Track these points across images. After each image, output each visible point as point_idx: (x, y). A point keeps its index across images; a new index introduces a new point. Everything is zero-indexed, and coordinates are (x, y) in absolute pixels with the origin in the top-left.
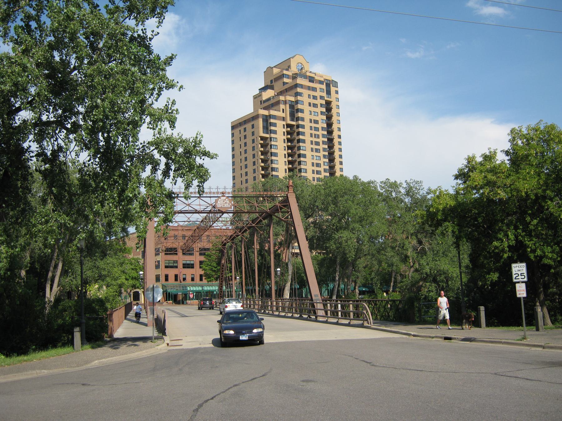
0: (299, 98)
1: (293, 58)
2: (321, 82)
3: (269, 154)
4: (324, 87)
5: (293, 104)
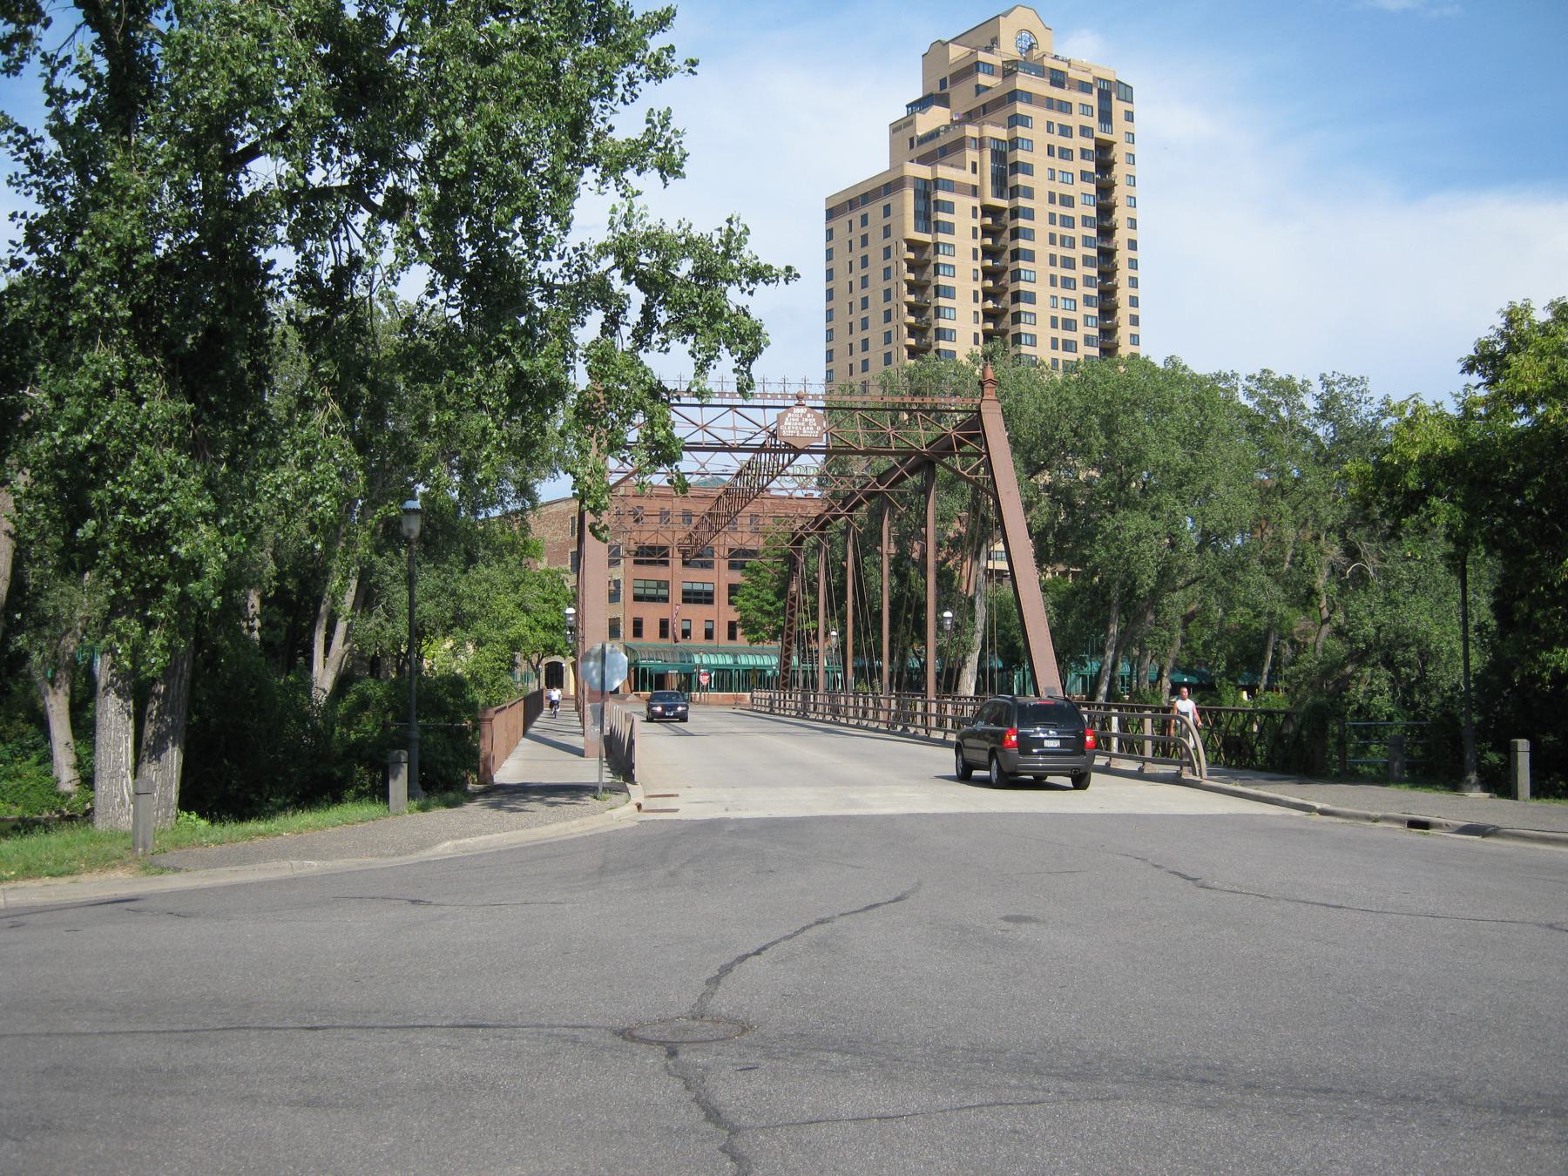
0: (1021, 131)
1: (1005, 15)
2: (1085, 87)
3: (931, 291)
4: (1092, 100)
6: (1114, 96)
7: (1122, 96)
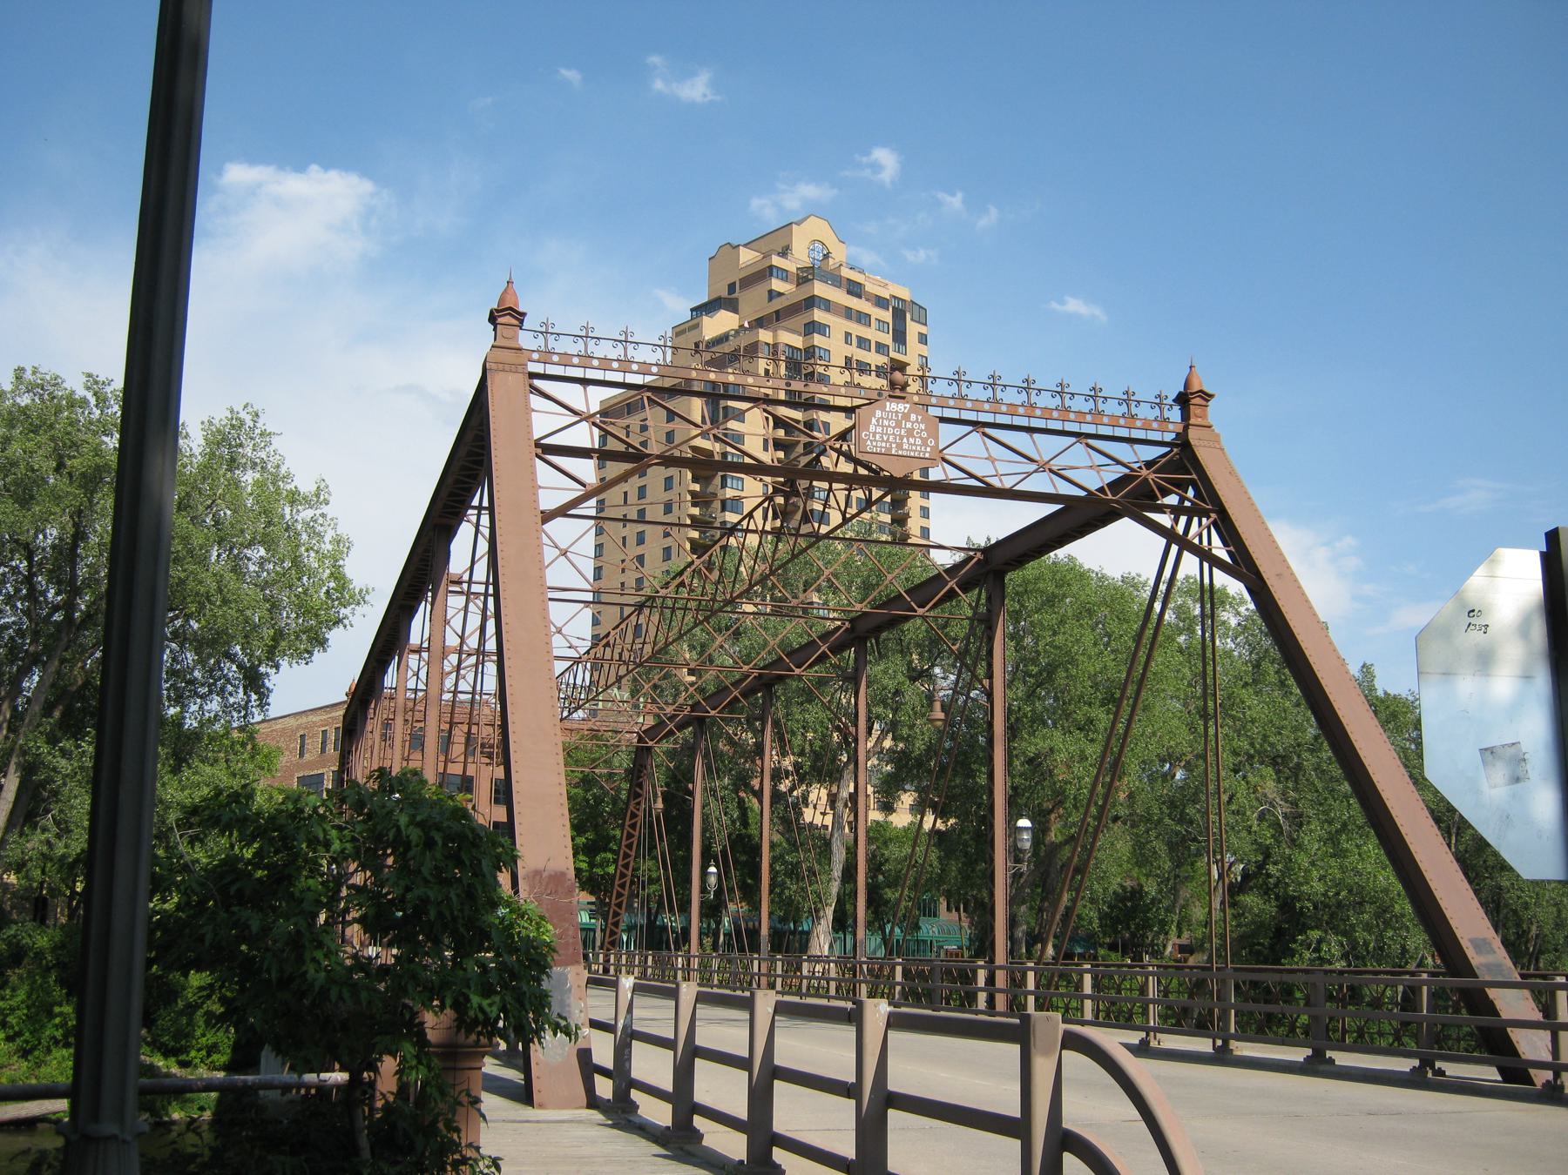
0: (818, 340)
1: (798, 224)
2: (881, 302)
3: (717, 505)
4: (887, 316)
5: (797, 356)
6: (908, 316)
7: (916, 318)
